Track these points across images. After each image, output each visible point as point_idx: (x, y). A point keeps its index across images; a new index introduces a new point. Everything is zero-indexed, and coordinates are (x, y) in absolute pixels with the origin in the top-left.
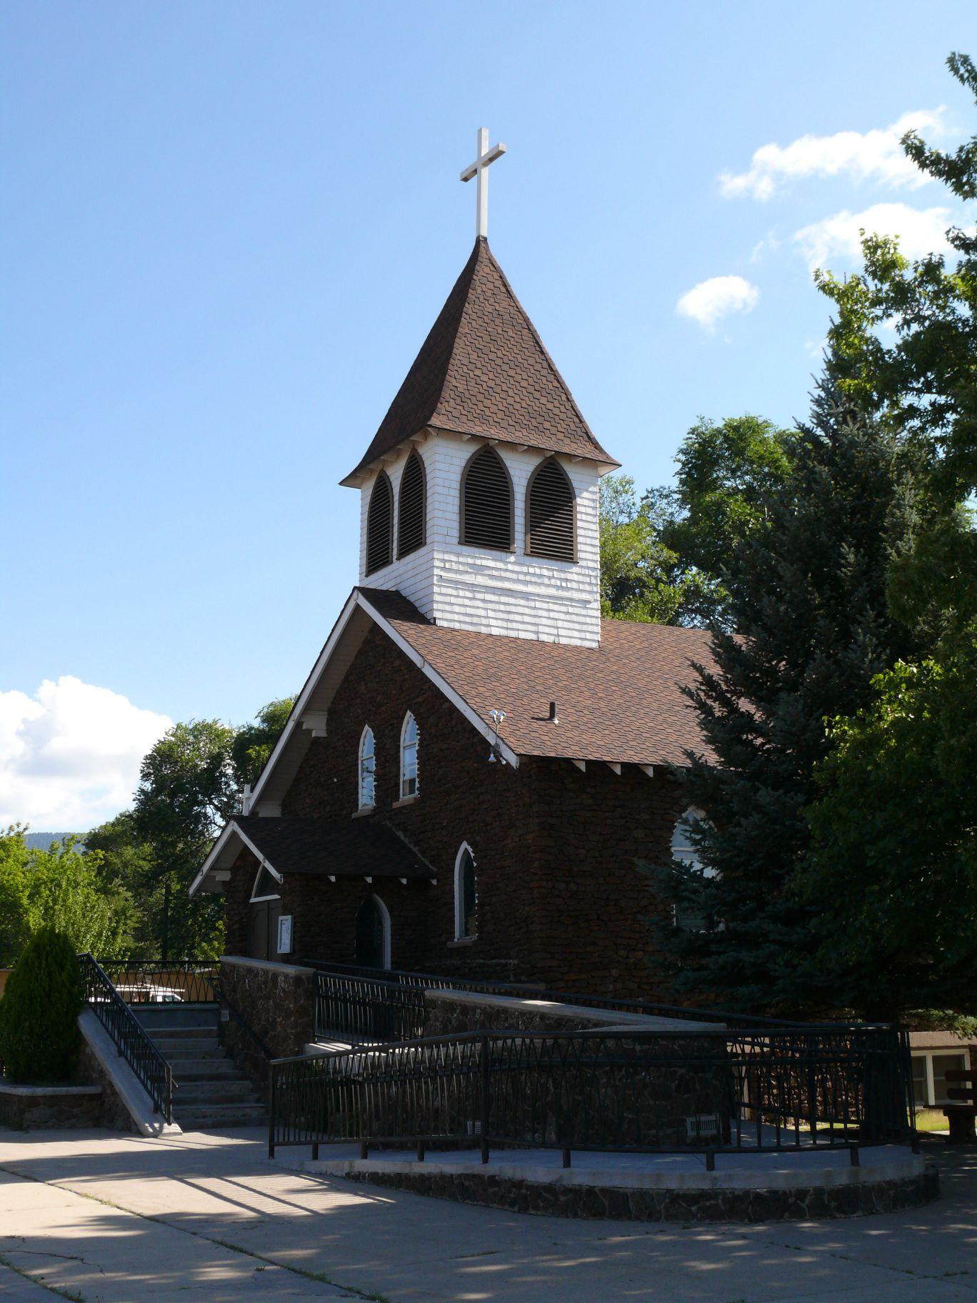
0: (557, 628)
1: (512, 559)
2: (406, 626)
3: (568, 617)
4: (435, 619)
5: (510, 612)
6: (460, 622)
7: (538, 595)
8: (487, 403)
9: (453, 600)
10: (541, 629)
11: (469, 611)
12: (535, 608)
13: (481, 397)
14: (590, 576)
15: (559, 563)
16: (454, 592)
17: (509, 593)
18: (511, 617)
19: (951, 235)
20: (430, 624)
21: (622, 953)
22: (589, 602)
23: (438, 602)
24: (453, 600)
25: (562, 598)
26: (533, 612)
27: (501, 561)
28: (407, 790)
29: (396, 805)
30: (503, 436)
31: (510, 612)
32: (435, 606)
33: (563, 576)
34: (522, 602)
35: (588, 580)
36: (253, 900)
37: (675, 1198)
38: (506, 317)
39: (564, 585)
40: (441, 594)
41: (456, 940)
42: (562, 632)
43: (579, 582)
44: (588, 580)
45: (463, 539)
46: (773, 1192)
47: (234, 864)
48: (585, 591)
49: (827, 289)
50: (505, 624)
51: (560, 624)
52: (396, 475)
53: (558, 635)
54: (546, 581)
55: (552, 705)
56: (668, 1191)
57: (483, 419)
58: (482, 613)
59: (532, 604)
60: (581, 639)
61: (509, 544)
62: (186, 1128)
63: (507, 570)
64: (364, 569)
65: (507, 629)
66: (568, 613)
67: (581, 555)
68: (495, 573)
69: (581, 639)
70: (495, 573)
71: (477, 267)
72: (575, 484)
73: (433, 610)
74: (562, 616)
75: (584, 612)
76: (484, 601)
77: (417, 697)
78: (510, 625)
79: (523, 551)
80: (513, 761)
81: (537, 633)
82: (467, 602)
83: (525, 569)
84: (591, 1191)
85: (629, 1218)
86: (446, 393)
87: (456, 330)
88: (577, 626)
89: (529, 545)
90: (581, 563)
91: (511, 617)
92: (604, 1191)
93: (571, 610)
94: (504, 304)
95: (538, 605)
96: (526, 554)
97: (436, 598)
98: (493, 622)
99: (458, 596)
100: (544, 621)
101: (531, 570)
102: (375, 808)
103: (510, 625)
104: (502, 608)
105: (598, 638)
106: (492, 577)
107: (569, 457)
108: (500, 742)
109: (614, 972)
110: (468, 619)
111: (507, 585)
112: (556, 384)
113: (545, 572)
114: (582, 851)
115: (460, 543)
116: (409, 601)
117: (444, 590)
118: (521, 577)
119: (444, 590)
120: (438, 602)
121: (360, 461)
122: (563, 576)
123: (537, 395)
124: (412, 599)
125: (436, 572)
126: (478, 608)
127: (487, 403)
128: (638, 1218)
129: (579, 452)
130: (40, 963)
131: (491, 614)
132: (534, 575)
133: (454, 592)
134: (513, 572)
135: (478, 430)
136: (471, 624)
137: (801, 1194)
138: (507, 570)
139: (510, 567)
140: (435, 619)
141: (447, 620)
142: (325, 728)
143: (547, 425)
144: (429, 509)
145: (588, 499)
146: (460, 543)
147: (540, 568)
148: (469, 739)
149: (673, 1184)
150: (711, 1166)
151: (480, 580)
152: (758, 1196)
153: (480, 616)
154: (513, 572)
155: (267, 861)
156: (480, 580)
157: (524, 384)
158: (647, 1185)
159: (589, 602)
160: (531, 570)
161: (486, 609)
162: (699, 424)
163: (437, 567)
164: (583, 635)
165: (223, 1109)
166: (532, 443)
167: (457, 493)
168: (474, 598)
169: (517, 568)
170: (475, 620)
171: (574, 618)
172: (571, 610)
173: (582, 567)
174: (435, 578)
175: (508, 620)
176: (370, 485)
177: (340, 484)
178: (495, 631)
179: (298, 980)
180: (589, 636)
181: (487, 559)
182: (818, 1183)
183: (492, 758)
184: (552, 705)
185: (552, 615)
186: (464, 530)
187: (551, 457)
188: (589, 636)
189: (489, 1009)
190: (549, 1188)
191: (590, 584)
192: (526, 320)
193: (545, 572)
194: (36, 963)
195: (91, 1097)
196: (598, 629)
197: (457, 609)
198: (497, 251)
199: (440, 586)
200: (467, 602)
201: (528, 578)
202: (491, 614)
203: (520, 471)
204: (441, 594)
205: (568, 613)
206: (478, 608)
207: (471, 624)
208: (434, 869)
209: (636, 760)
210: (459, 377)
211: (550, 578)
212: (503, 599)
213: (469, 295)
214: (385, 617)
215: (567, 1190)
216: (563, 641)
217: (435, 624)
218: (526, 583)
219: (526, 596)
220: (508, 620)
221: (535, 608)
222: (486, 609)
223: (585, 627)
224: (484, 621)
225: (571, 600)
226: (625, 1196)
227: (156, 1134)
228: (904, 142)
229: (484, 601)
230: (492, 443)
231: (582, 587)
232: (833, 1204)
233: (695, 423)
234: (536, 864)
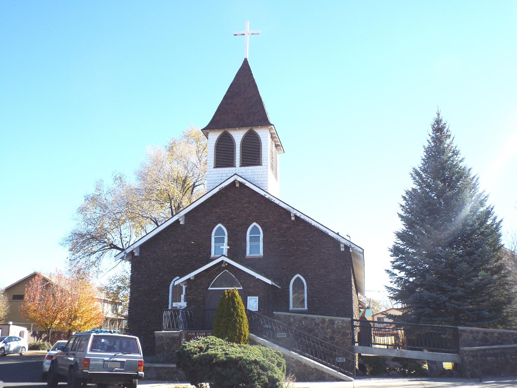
36: (210, 289)
77: (264, 219)
176: (214, 136)
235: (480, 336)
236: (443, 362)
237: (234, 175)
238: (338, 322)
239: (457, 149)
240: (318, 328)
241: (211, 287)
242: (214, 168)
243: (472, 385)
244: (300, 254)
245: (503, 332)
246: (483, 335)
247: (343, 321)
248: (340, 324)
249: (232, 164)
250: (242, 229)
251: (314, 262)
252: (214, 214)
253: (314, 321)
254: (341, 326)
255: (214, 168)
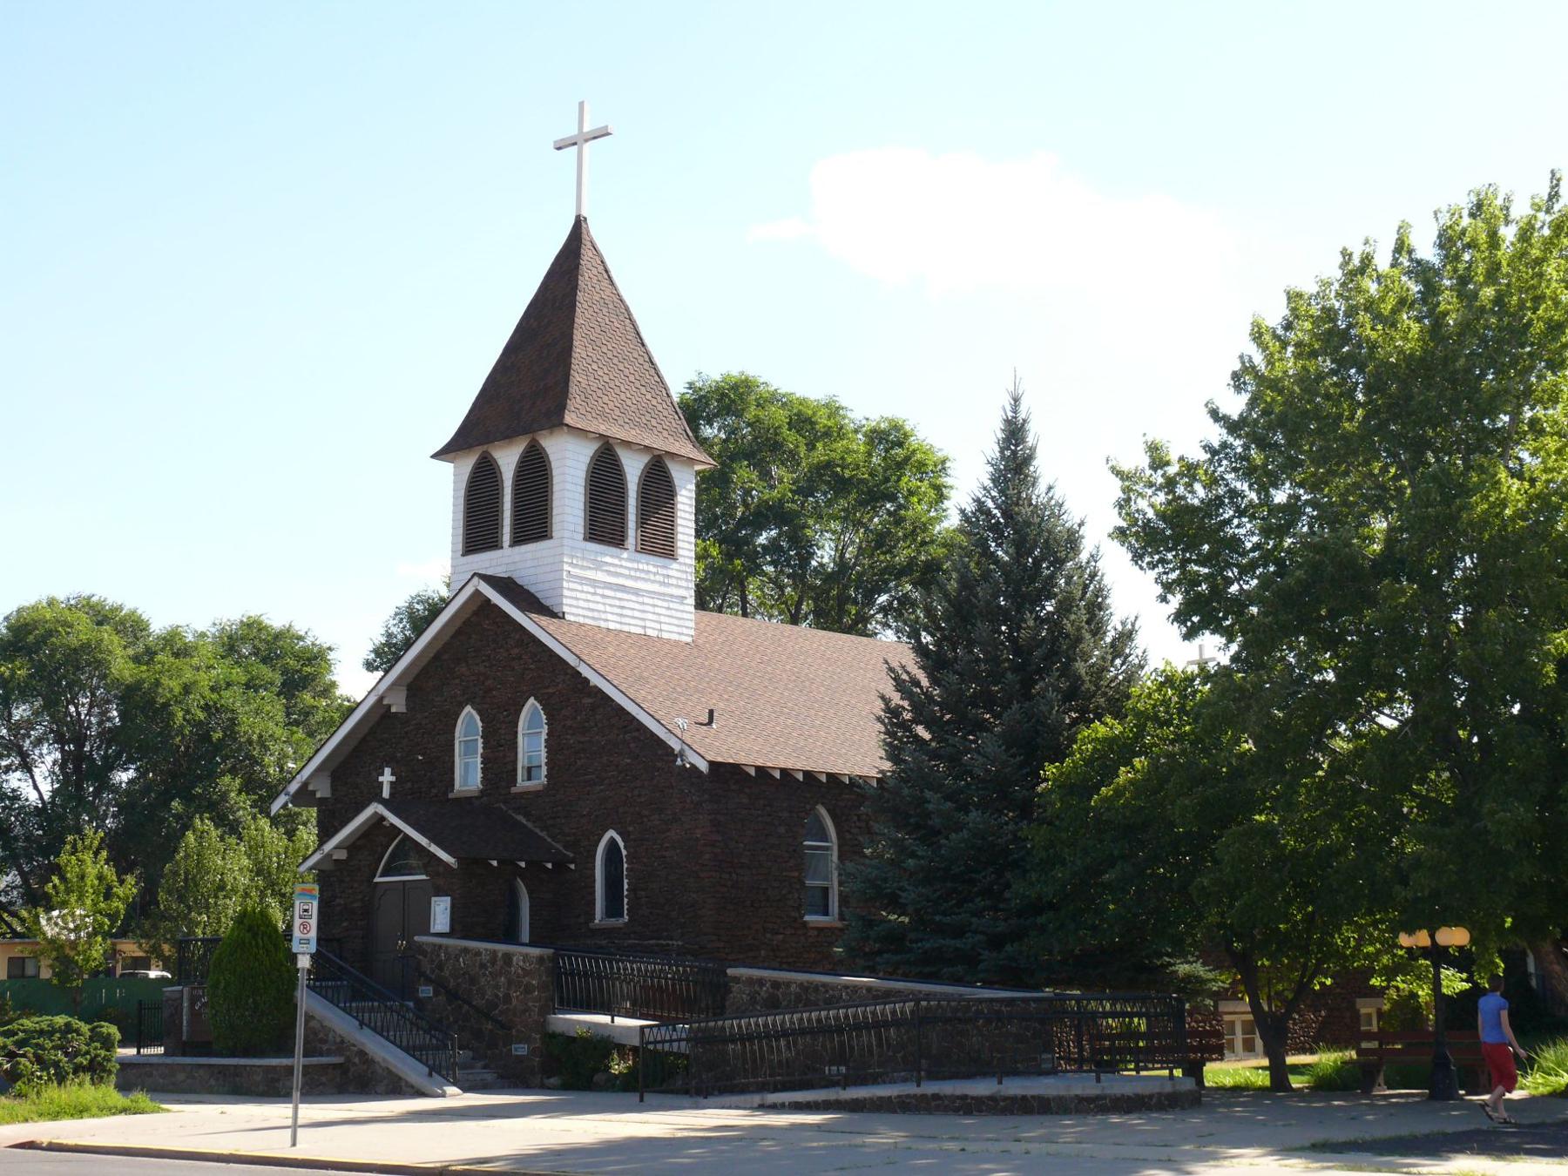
0: (661, 623)
1: (625, 555)
2: (544, 620)
3: (669, 613)
4: (564, 613)
5: (623, 607)
6: (584, 616)
7: (646, 591)
8: (605, 399)
9: (579, 595)
10: (648, 624)
11: (592, 606)
12: (643, 603)
13: (599, 393)
14: (687, 572)
15: (662, 559)
16: (579, 588)
17: (623, 588)
18: (625, 612)
19: (1203, 444)
20: (560, 618)
21: (768, 936)
22: (686, 598)
23: (566, 597)
24: (579, 595)
25: (664, 594)
26: (641, 607)
27: (617, 557)
28: (525, 778)
29: (514, 790)
30: (622, 435)
31: (623, 607)
32: (565, 601)
33: (665, 572)
34: (634, 598)
35: (684, 576)
36: (377, 879)
37: (1081, 1100)
38: (611, 306)
39: (666, 581)
40: (568, 589)
41: (597, 921)
42: (664, 627)
43: (678, 578)
44: (684, 576)
45: (588, 535)
46: (1137, 1095)
47: (354, 843)
48: (682, 587)
49: (1118, 473)
50: (618, 619)
51: (663, 619)
52: (508, 459)
53: (661, 630)
54: (652, 577)
55: (711, 712)
56: (1077, 1096)
57: (603, 416)
58: (600, 607)
59: (640, 599)
60: (679, 633)
61: (623, 541)
62: (465, 1089)
63: (621, 566)
64: (460, 546)
65: (621, 623)
66: (668, 608)
67: (680, 552)
68: (612, 569)
69: (679, 633)
70: (612, 569)
71: (582, 251)
72: (677, 482)
73: (562, 604)
74: (663, 611)
75: (681, 608)
76: (603, 596)
77: (547, 687)
78: (624, 620)
79: (634, 548)
80: (703, 766)
81: (645, 627)
82: (590, 597)
83: (635, 566)
84: (1024, 1098)
85: (1052, 1114)
86: (573, 389)
87: (573, 322)
88: (676, 622)
89: (639, 542)
90: (681, 560)
91: (625, 612)
92: (1033, 1097)
93: (672, 605)
94: (608, 292)
95: (646, 600)
96: (637, 551)
97: (566, 593)
98: (610, 617)
99: (582, 591)
100: (650, 616)
101: (641, 566)
102: (481, 791)
103: (624, 620)
104: (617, 603)
105: (692, 632)
106: (608, 572)
107: (673, 455)
108: (686, 747)
109: (763, 952)
110: (590, 614)
111: (621, 581)
112: (657, 378)
113: (651, 568)
114: (742, 845)
115: (585, 539)
116: (528, 592)
117: (572, 586)
118: (633, 573)
119: (572, 586)
120: (566, 597)
121: (449, 439)
122: (665, 572)
123: (643, 390)
124: (532, 590)
125: (566, 567)
126: (598, 603)
127: (605, 399)
128: (1057, 1113)
129: (682, 452)
130: (257, 943)
131: (608, 609)
132: (643, 571)
133: (579, 588)
134: (626, 568)
135: (602, 429)
136: (593, 618)
137: (1151, 1097)
138: (621, 566)
139: (624, 563)
140: (564, 613)
141: (573, 614)
142: (404, 702)
143: (654, 422)
144: (556, 503)
145: (687, 497)
146: (585, 539)
147: (648, 564)
148: (618, 735)
149: (1079, 1092)
150: (1098, 1080)
151: (601, 576)
152: (1129, 1097)
153: (599, 611)
154: (626, 568)
155: (433, 845)
156: (601, 576)
157: (632, 378)
158: (1062, 1093)
159: (686, 598)
160: (641, 566)
161: (604, 604)
162: (696, 379)
163: (567, 563)
164: (680, 630)
165: (468, 1074)
166: (647, 443)
167: (582, 490)
168: (595, 594)
169: (629, 565)
170: (596, 615)
171: (673, 613)
172: (672, 605)
173: (680, 564)
174: (565, 573)
175: (621, 615)
176: (468, 463)
177: (433, 457)
178: (612, 626)
179: (541, 959)
180: (685, 631)
181: (608, 556)
182: (1157, 1090)
183: (679, 762)
184: (711, 712)
185: (657, 610)
186: (588, 526)
187: (659, 456)
188: (685, 631)
189: (806, 984)
190: (992, 1098)
191: (687, 580)
192: (627, 309)
193: (651, 568)
194: (254, 943)
195: (334, 1066)
196: (692, 624)
197: (582, 604)
198: (597, 231)
199: (568, 581)
200: (590, 597)
201: (638, 574)
202: (608, 609)
203: (633, 468)
204: (568, 589)
205: (668, 608)
206: (598, 603)
207: (593, 618)
208: (571, 855)
209: (790, 766)
210: (580, 371)
211: (655, 574)
212: (619, 595)
213: (580, 282)
214: (523, 611)
215: (1005, 1099)
216: (665, 635)
217: (564, 618)
218: (637, 579)
219: (636, 592)
220: (621, 615)
221: (643, 603)
222: (604, 604)
223: (681, 623)
224: (603, 616)
225: (672, 596)
226: (1048, 1099)
227: (443, 1095)
228: (1206, 405)
229: (603, 596)
230: (611, 441)
231: (680, 583)
232: (1166, 1103)
233: (693, 377)
234: (707, 856)
235: (764, 992)
236: (1262, 1089)
237: (472, 577)
238: (518, 960)
239: (1274, 316)
240: (484, 975)
241: (381, 876)
242: (463, 555)
243: (1360, 1169)
244: (613, 776)
245: (808, 982)
246: (771, 990)
247: (526, 956)
248: (521, 964)
249: (493, 544)
250: (508, 716)
251: (639, 796)
252: (457, 681)
253: (478, 958)
254: (523, 969)
255: (463, 555)
